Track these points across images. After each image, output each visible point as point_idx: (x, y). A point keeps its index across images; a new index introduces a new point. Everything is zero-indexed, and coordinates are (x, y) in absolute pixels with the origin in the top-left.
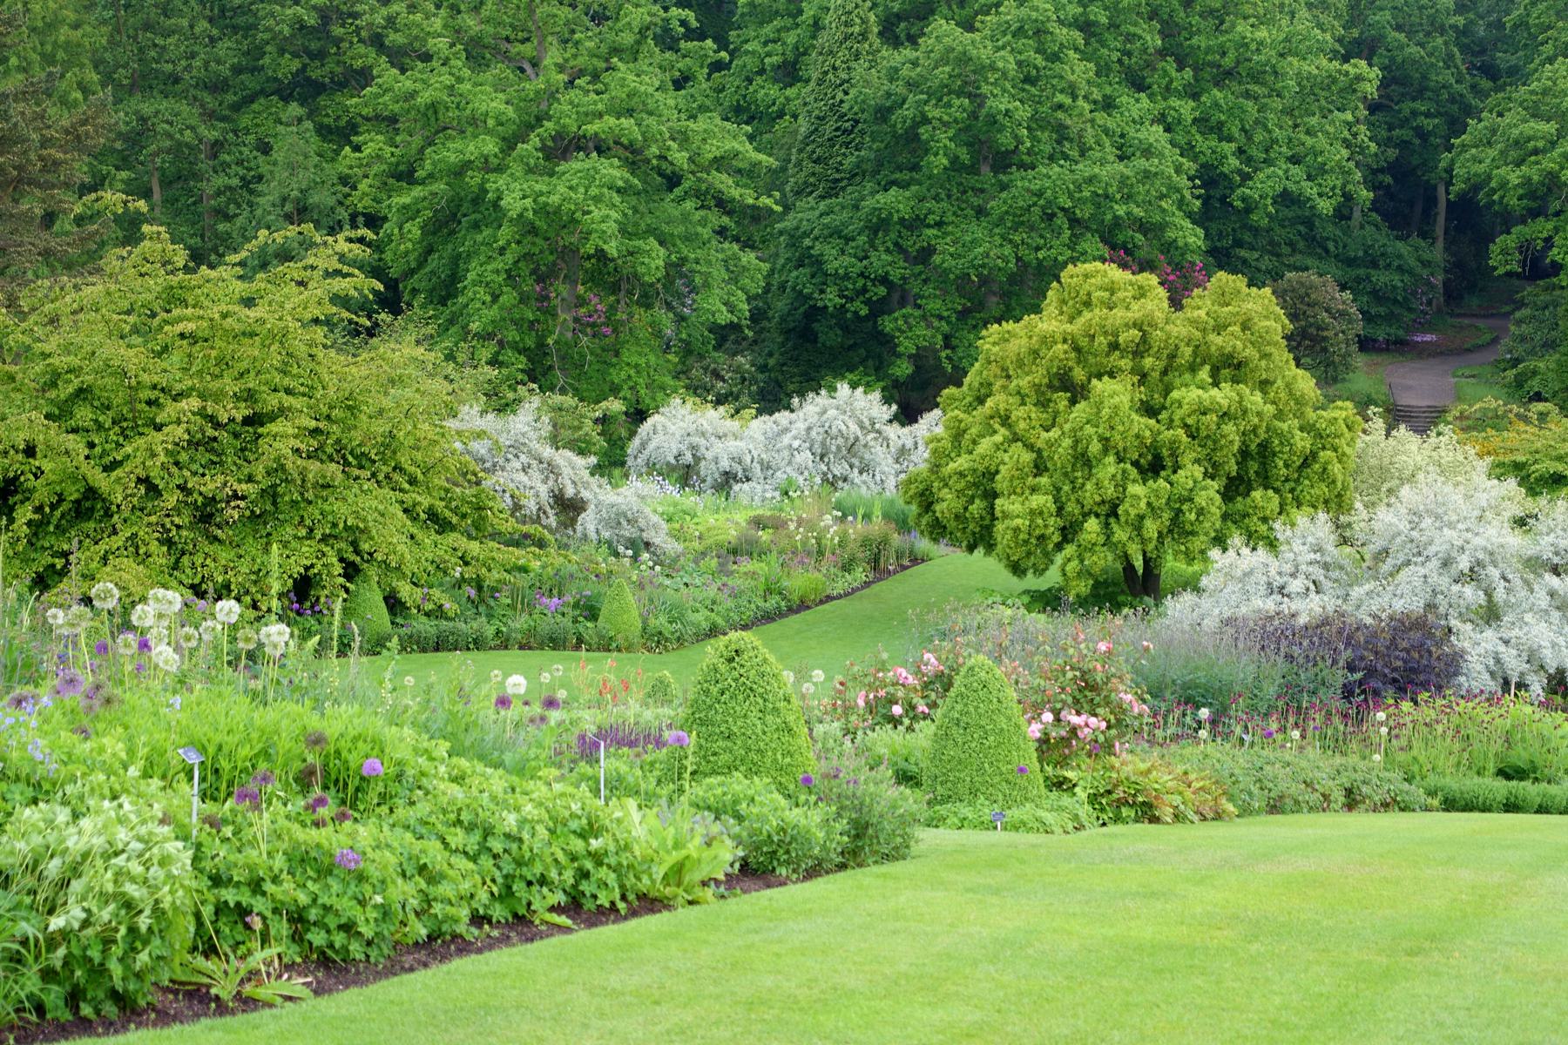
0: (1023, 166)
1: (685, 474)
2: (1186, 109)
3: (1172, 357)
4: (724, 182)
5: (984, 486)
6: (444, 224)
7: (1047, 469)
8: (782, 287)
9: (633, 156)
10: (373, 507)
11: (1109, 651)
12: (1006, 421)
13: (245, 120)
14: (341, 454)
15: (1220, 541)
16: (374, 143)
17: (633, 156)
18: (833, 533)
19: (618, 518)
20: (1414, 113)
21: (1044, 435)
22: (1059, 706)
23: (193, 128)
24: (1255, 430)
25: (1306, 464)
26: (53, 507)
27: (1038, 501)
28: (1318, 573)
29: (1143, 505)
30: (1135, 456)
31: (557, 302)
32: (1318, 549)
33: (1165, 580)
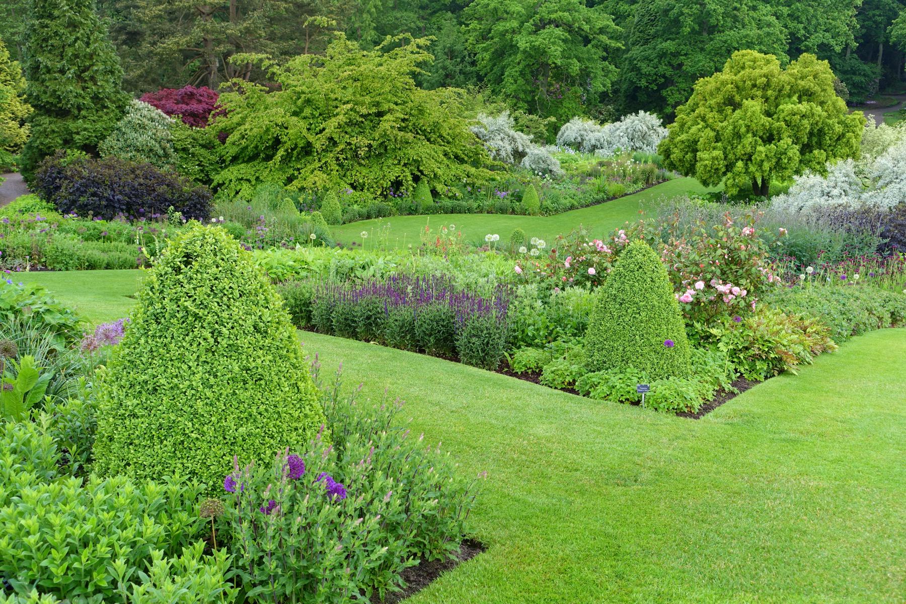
0: (719, 32)
1: (578, 145)
2: (785, 10)
3: (780, 91)
4: (604, 38)
5: (692, 147)
6: (499, 55)
7: (721, 140)
8: (625, 79)
9: (569, 28)
10: (422, 150)
11: (752, 235)
12: (704, 119)
13: (434, 20)
14: (417, 131)
15: (798, 172)
16: (474, 24)
17: (569, 28)
18: (630, 170)
19: (538, 160)
20: (874, 15)
21: (720, 124)
22: (709, 276)
23: (414, 22)
24: (817, 124)
25: (838, 139)
26: (293, 150)
27: (716, 153)
28: (846, 187)
29: (763, 155)
30: (761, 134)
31: (539, 83)
32: (847, 176)
33: (771, 190)
